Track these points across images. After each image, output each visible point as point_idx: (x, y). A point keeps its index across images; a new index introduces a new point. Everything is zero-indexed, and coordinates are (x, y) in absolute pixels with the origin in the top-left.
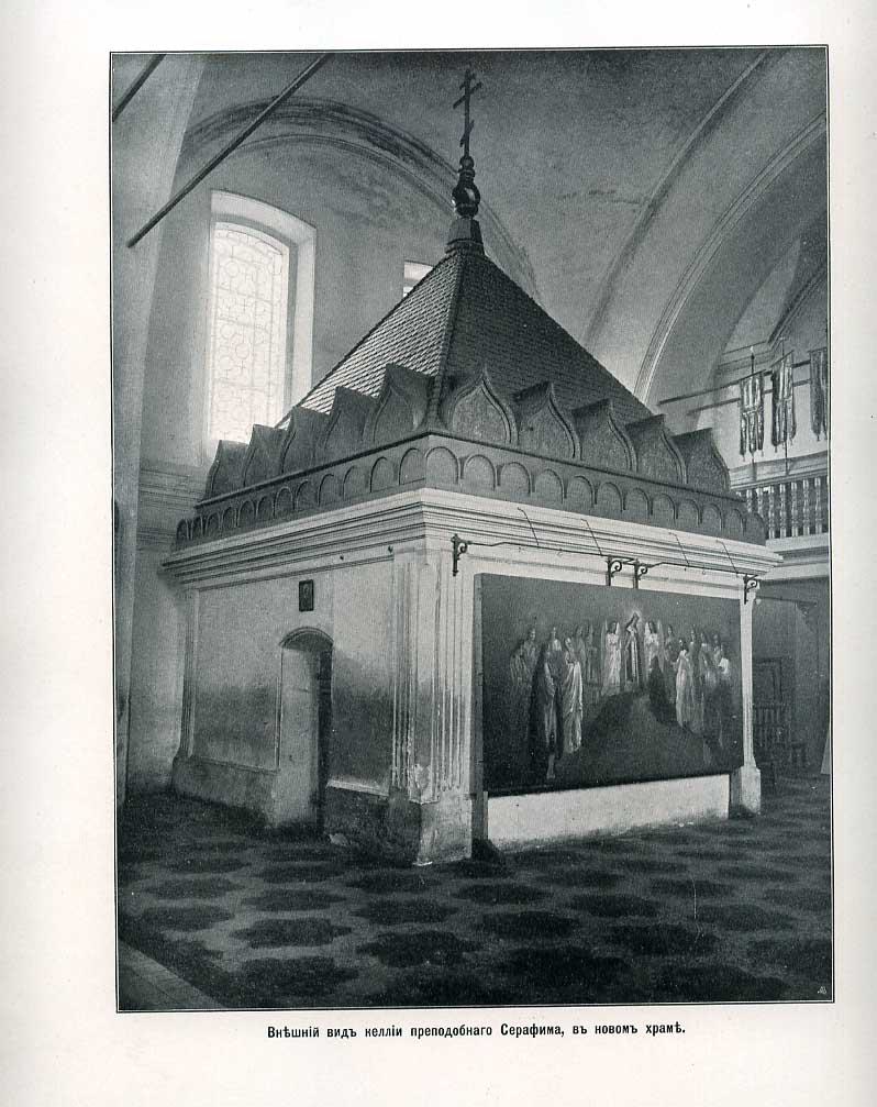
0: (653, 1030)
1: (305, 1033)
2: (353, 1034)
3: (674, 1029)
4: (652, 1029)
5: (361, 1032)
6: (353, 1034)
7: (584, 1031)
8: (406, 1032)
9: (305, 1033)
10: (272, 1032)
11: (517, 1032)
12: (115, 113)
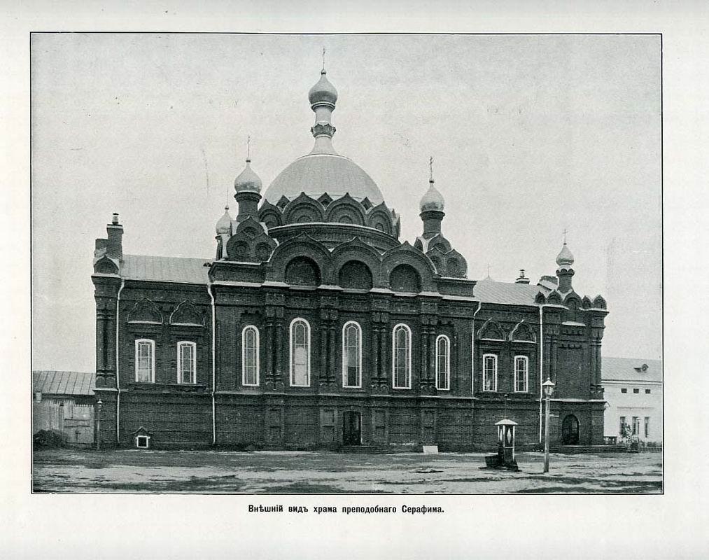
0: (319, 510)
1: (273, 509)
2: (306, 510)
3: (259, 509)
4: (317, 509)
5: (311, 510)
6: (306, 510)
9: (273, 509)
10: (251, 508)
11: (413, 510)
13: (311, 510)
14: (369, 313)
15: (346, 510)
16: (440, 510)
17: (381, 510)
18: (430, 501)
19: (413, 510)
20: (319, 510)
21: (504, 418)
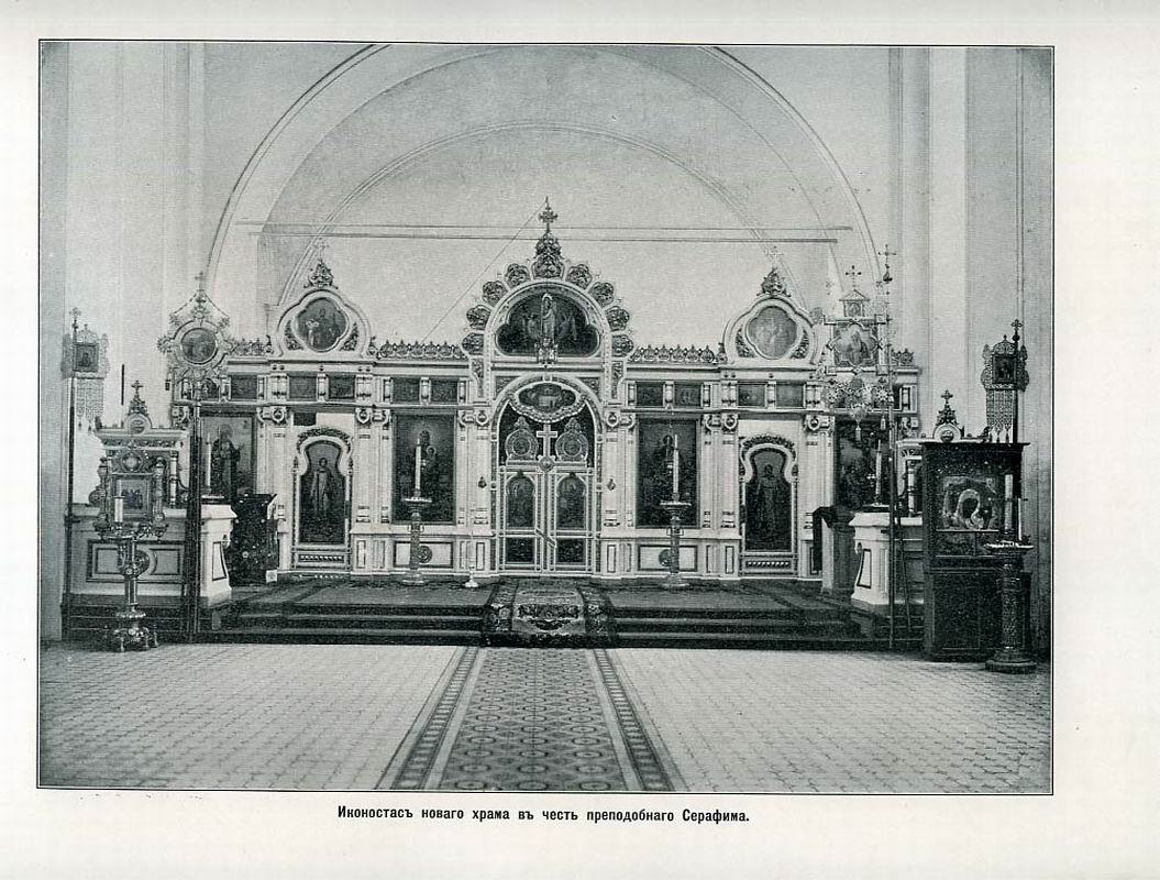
0: (480, 815)
2: (409, 815)
4: (478, 814)
7: (530, 817)
8: (469, 815)
10: (342, 811)
11: (699, 817)
12: (717, 47)
13: (582, 816)
14: (803, 417)
15: (594, 816)
16: (743, 818)
17: (649, 816)
18: (727, 804)
19: (699, 817)
20: (480, 815)
21: (267, 504)
